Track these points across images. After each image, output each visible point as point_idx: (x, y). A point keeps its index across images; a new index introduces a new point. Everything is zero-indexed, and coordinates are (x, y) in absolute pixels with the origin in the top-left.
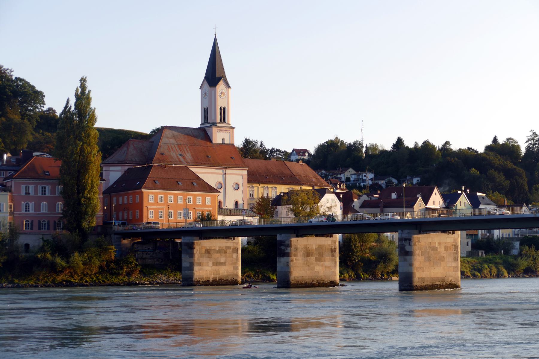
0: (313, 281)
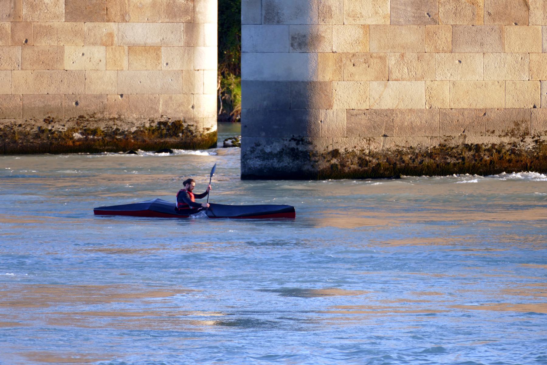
0: (48, 121)
